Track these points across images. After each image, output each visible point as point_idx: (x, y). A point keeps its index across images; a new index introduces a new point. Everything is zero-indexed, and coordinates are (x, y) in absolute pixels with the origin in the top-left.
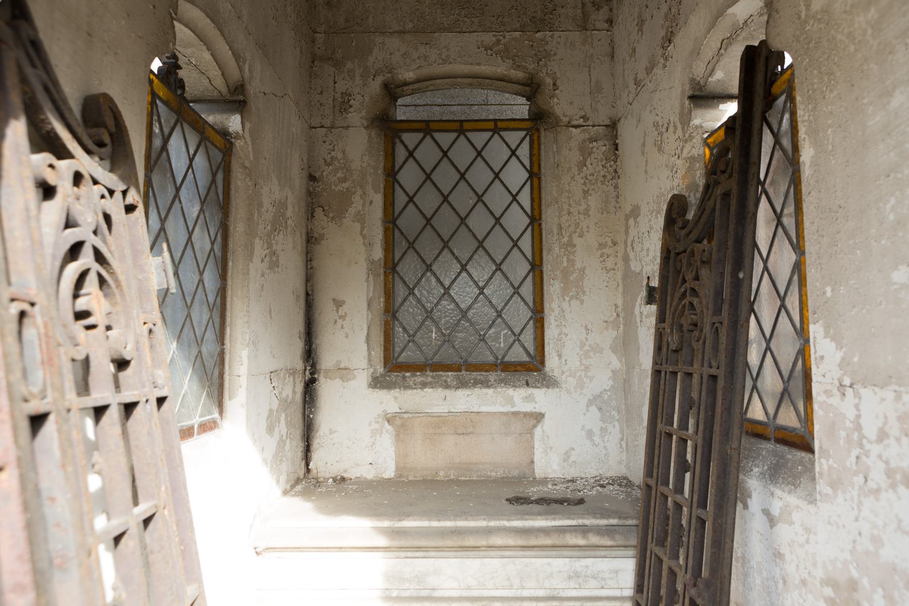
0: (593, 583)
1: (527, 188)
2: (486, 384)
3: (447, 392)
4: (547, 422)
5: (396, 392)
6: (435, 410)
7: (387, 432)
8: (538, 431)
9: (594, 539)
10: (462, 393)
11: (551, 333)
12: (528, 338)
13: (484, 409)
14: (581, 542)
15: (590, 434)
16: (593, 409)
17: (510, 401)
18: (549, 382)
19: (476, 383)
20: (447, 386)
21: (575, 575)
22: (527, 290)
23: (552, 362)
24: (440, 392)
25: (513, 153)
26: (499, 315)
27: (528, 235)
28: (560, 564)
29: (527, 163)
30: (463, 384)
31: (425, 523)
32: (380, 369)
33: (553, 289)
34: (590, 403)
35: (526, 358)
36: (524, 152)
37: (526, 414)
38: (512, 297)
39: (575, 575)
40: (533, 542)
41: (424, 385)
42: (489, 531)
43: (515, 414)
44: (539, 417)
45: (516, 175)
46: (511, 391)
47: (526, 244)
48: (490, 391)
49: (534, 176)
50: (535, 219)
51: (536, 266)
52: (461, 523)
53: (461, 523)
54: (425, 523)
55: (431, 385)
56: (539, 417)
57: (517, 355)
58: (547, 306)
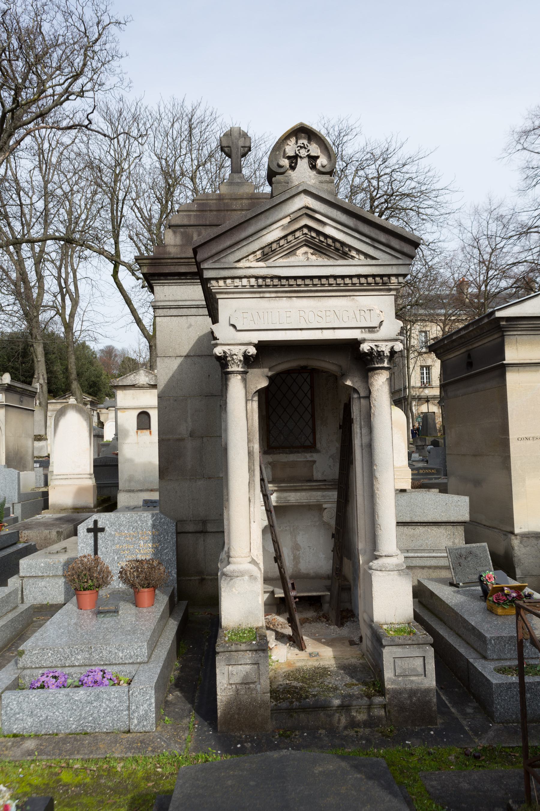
0: (328, 498)
1: (310, 406)
2: (298, 452)
3: (287, 455)
4: (317, 464)
5: (271, 455)
6: (283, 460)
7: (143, 587)
8: (315, 466)
9: (327, 487)
10: (291, 455)
11: (318, 436)
12: (311, 438)
13: (298, 460)
14: (324, 487)
15: (330, 466)
16: (331, 459)
17: (306, 457)
18: (317, 451)
19: (295, 452)
20: (287, 453)
21: (323, 496)
22: (310, 423)
23: (318, 445)
24: (285, 455)
25: (305, 380)
26: (302, 431)
27: (310, 392)
28: (319, 493)
29: (309, 383)
30: (291, 453)
31: (286, 485)
32: (266, 449)
33: (318, 423)
34: (330, 457)
35: (310, 444)
36: (308, 380)
37: (311, 461)
38: (55, 315)
39: (323, 496)
40: (313, 488)
41: (280, 453)
42: (302, 486)
43: (307, 461)
44: (314, 462)
45: (306, 388)
46: (306, 454)
47: (310, 409)
48: (300, 454)
49: (312, 387)
50: (312, 401)
51: (313, 416)
52: (295, 485)
53: (295, 485)
54: (286, 485)
55: (282, 453)
56: (314, 462)
57: (308, 443)
58: (316, 428)
